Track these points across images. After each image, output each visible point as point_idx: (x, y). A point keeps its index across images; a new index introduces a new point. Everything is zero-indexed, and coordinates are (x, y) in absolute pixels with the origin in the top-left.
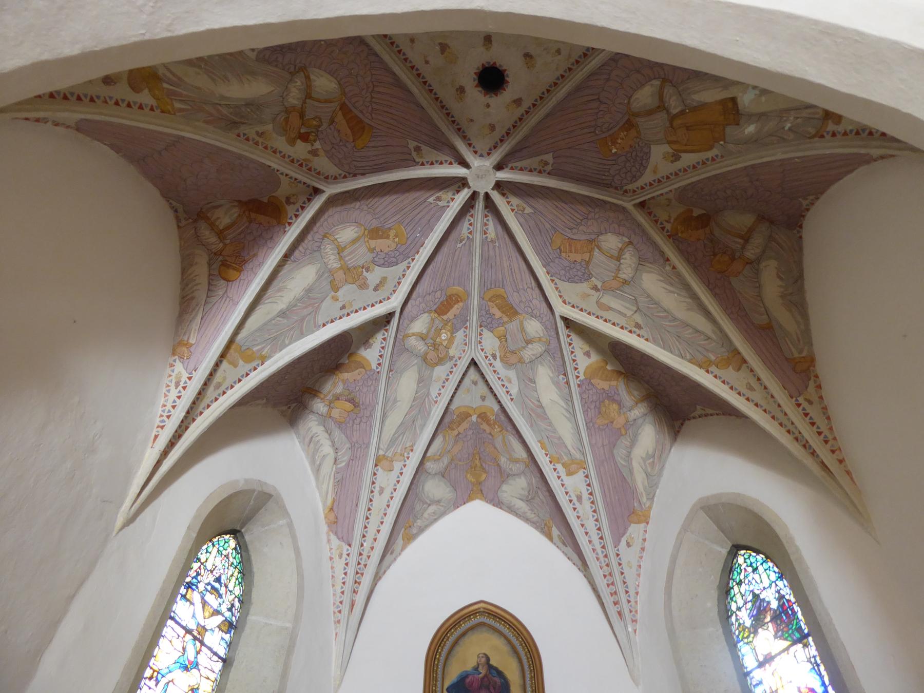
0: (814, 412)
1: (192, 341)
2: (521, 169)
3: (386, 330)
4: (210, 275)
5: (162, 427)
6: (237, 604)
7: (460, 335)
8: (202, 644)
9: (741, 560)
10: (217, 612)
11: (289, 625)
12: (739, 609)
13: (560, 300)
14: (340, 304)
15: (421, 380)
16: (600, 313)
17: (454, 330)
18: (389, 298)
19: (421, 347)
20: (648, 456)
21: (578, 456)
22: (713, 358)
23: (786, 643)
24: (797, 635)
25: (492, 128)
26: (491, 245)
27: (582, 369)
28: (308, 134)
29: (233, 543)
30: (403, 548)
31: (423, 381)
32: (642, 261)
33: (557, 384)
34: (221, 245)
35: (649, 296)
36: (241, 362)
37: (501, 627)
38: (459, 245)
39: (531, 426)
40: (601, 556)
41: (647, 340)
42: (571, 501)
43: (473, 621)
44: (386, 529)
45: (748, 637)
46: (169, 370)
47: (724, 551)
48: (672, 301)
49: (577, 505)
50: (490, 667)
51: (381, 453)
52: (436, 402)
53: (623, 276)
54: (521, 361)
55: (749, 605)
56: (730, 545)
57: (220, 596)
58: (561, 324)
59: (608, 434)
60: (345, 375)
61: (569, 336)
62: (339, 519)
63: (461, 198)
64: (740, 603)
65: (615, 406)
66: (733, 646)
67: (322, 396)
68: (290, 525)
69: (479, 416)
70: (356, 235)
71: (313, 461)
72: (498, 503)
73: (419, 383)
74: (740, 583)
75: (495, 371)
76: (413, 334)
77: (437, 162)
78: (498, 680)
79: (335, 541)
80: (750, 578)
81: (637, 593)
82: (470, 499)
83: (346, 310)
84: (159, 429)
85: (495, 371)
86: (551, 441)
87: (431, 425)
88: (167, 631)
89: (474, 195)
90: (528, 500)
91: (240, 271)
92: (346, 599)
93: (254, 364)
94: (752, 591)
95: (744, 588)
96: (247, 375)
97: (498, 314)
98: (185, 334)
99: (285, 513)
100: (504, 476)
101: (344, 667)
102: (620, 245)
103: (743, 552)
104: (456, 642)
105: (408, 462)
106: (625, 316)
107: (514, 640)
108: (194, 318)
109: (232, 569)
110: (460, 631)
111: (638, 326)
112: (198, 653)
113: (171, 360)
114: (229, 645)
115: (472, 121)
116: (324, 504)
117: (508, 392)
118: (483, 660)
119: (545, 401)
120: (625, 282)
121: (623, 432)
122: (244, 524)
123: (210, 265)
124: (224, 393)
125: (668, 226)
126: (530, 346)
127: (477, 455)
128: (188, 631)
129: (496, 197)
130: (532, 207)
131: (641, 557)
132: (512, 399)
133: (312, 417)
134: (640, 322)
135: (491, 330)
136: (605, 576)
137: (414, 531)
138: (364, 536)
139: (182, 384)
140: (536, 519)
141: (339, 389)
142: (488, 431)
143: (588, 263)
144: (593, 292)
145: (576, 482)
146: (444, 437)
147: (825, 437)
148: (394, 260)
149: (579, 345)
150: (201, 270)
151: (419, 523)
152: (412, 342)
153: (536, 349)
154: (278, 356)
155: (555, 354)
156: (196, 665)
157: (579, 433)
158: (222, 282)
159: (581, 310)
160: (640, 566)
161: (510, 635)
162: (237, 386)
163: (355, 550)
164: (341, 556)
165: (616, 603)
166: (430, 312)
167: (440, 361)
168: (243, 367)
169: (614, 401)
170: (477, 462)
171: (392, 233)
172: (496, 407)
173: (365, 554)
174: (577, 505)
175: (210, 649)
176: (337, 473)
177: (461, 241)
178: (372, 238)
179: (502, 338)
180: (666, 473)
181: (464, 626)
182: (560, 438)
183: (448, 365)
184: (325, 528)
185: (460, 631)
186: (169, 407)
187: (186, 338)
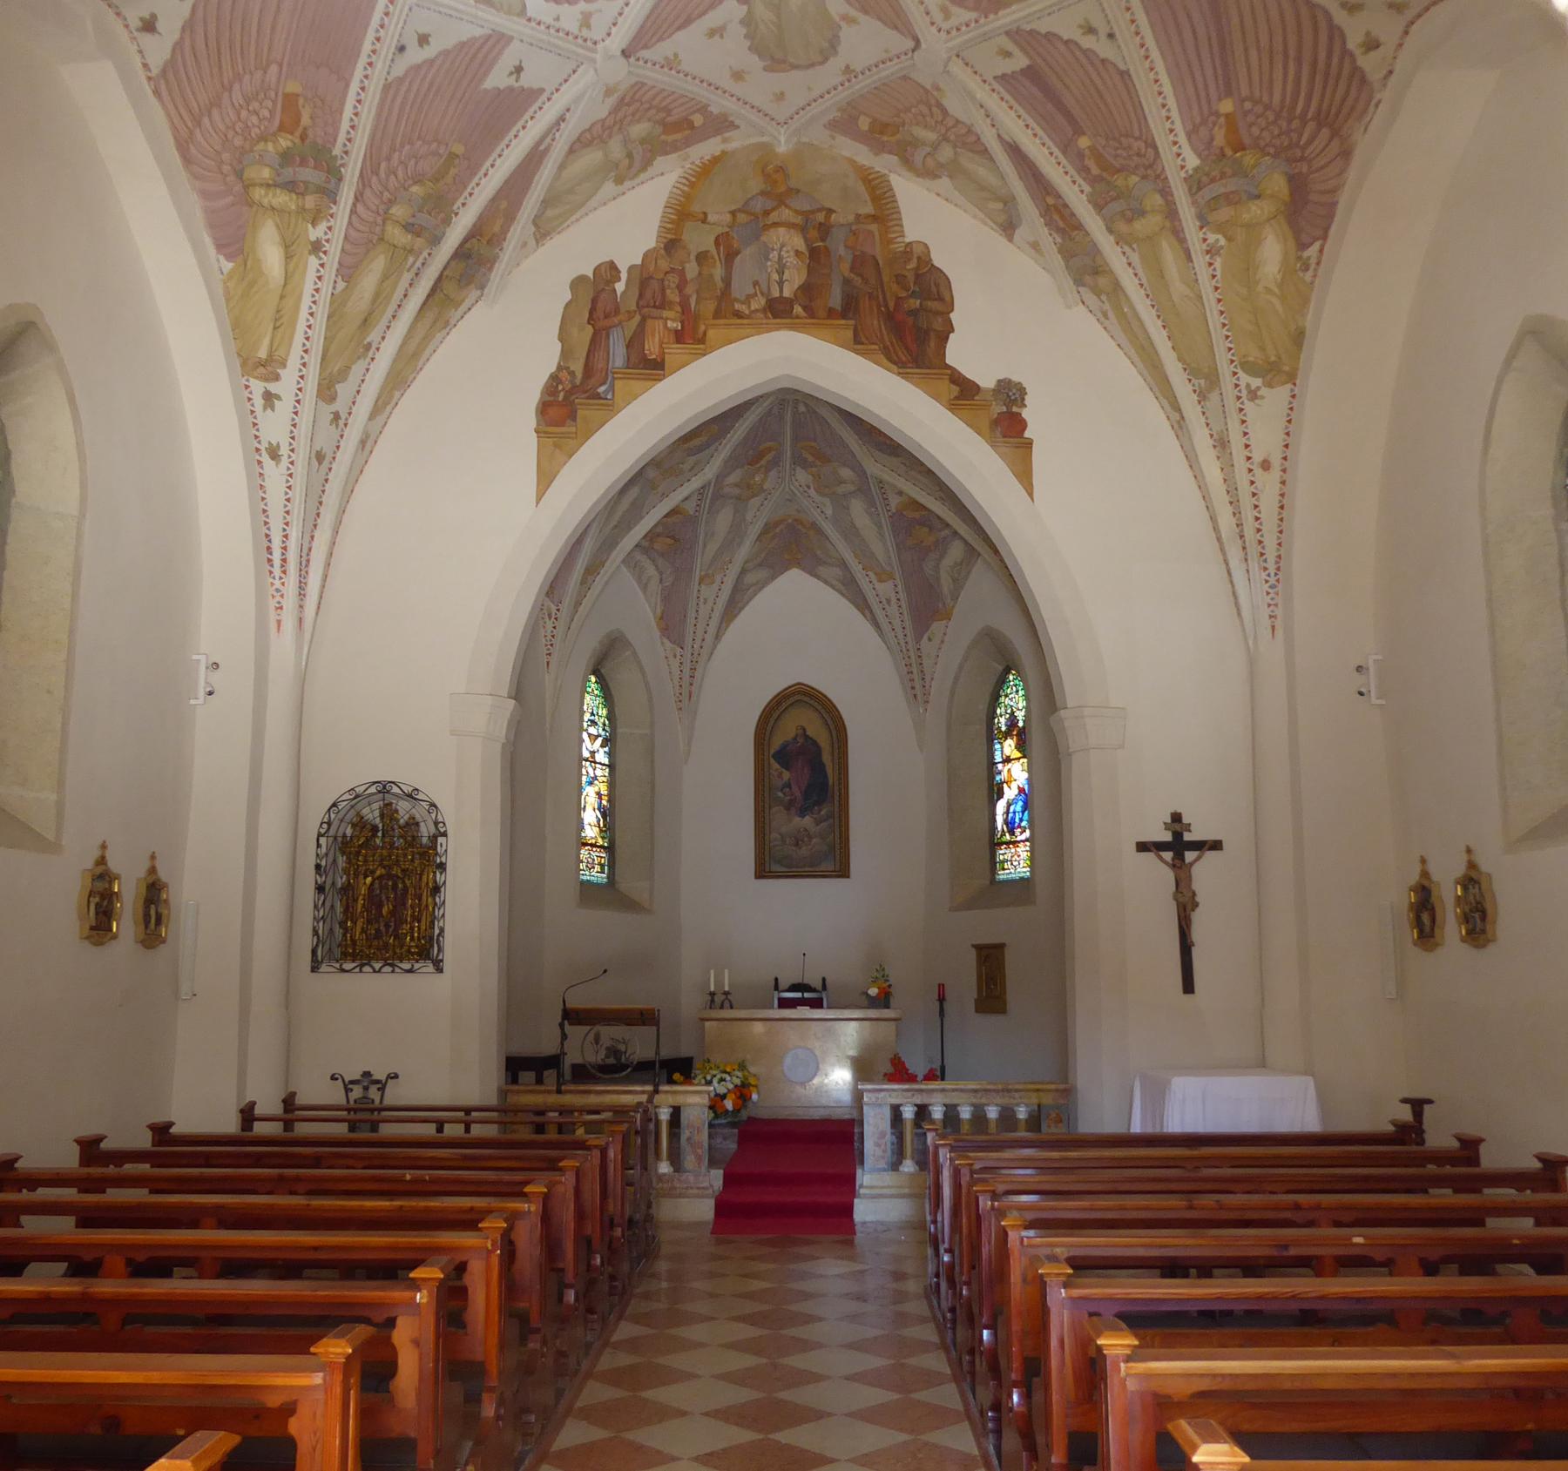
7: (773, 473)
17: (768, 471)
19: (737, 491)
23: (1019, 755)
43: (792, 700)
44: (714, 623)
47: (1001, 668)
62: (671, 625)
65: (926, 529)
68: (635, 654)
71: (639, 580)
95: (1007, 701)
97: (810, 459)
119: (858, 523)
145: (885, 588)
156: (595, 778)
181: (784, 705)
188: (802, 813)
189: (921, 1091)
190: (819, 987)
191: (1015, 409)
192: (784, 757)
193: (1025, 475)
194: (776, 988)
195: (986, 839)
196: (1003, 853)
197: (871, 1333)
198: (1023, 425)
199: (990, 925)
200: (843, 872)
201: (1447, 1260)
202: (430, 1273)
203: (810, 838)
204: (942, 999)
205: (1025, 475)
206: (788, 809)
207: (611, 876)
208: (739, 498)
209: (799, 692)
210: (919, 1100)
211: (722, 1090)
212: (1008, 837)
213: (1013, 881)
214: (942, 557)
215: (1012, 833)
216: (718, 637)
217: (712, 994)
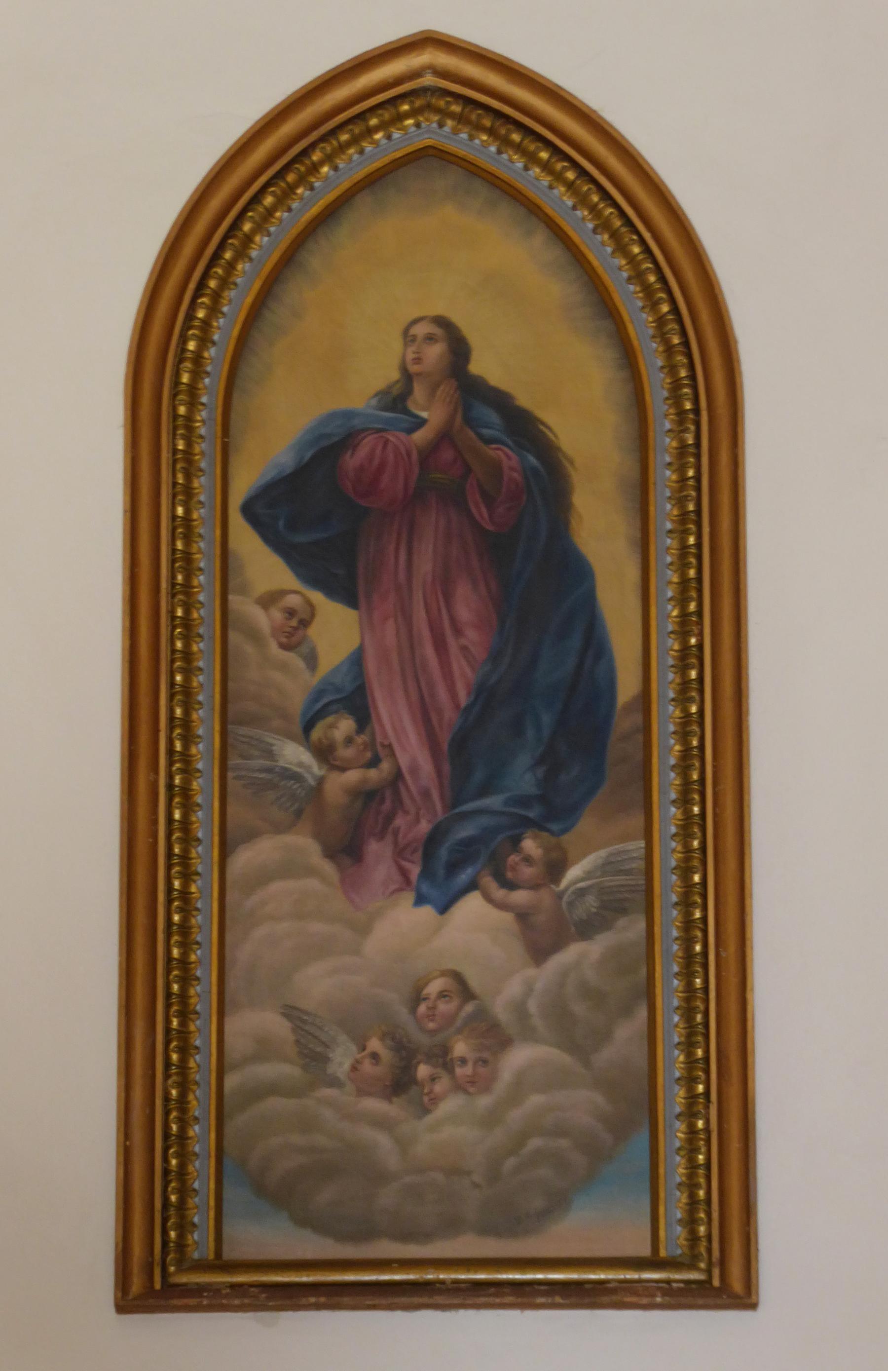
37: (535, 181)
43: (382, 147)
50: (471, 391)
78: (509, 459)
104: (290, 259)
107: (600, 251)
110: (307, 204)
118: (435, 352)
161: (580, 224)
181: (330, 180)
185: (307, 204)
188: (442, 872)
192: (325, 512)
197: (243, 730)
201: (614, 1291)
202: (131, 1297)
203: (494, 1038)
206: (346, 851)
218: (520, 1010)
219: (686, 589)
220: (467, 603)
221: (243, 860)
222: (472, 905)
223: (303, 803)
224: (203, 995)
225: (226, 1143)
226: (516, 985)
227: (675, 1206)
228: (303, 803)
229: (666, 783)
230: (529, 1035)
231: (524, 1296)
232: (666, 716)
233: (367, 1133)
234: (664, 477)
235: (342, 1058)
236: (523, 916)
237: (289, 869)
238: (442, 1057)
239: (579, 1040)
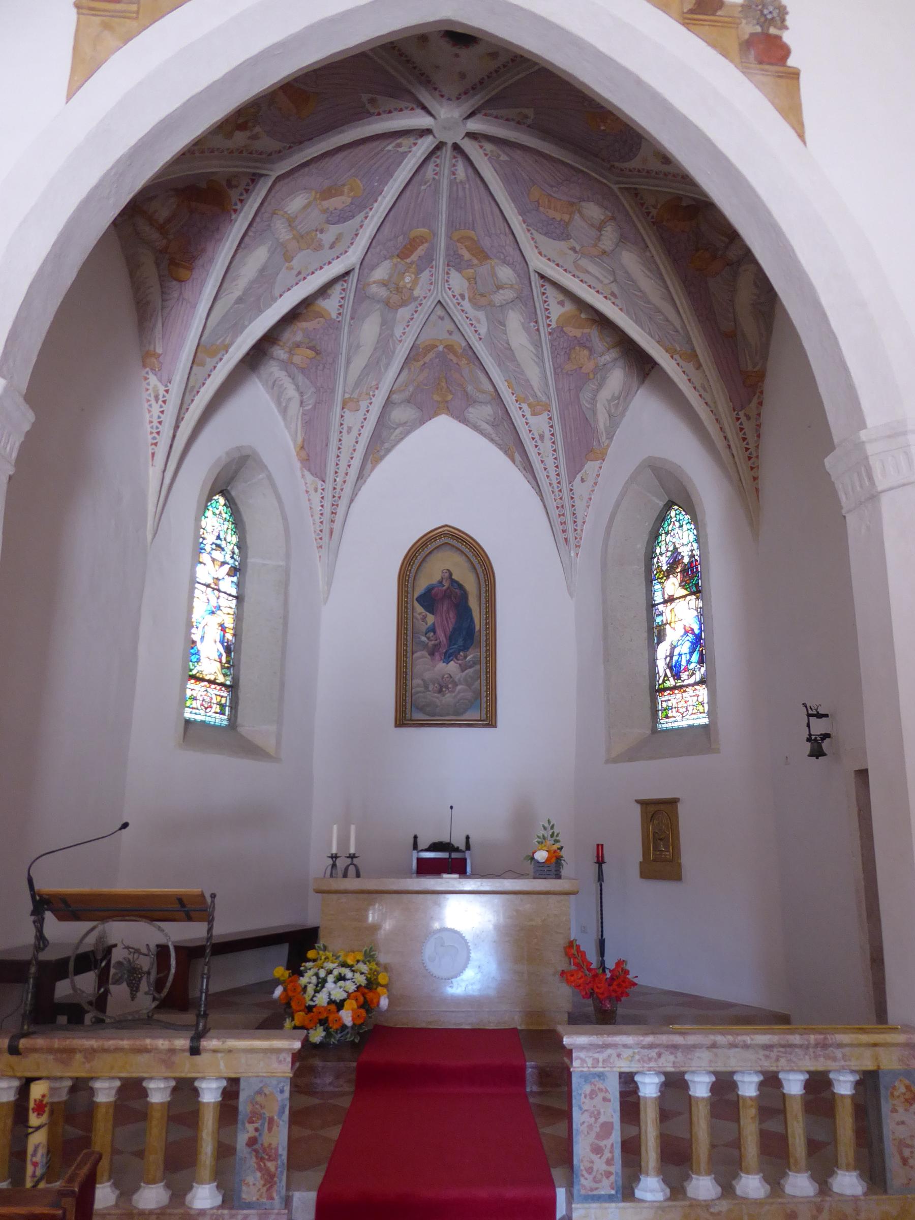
0: (748, 426)
1: (159, 350)
2: (496, 117)
3: (345, 281)
4: (160, 277)
5: (156, 444)
6: (236, 551)
7: (425, 275)
8: (219, 590)
9: (673, 513)
10: (223, 563)
11: (282, 563)
12: (661, 554)
13: (536, 251)
14: (295, 272)
15: (384, 323)
16: (577, 273)
17: (419, 271)
18: (346, 252)
19: (383, 293)
20: (614, 398)
21: (544, 399)
22: (678, 349)
23: (685, 592)
24: (694, 589)
25: (463, 76)
26: (460, 186)
27: (554, 316)
28: (246, 123)
29: (222, 501)
30: (372, 469)
31: (386, 324)
32: (623, 239)
33: (526, 329)
34: (165, 241)
35: (626, 272)
36: (208, 360)
37: (463, 548)
38: (423, 187)
39: (499, 366)
40: (556, 490)
41: (621, 309)
42: (533, 439)
44: (356, 463)
45: (662, 578)
46: (144, 383)
47: (661, 504)
48: (647, 284)
49: (539, 443)
50: (453, 581)
51: (347, 396)
52: (400, 341)
53: (603, 247)
54: (491, 304)
55: (669, 554)
56: (667, 499)
57: (223, 549)
58: (534, 278)
59: (574, 380)
60: (304, 325)
61: (543, 286)
62: (312, 456)
63: (425, 146)
64: (664, 549)
65: (586, 352)
66: (649, 582)
67: (281, 344)
68: (270, 477)
69: (445, 347)
70: (306, 201)
71: (278, 403)
72: (464, 421)
73: (382, 325)
74: (667, 533)
75: (463, 311)
76: (374, 282)
77: (395, 109)
79: (309, 477)
80: (675, 532)
81: (584, 523)
82: (436, 414)
83: (301, 276)
84: (153, 446)
85: (463, 311)
86: (518, 380)
87: (396, 365)
88: (197, 593)
89: (440, 146)
90: (494, 426)
91: (191, 269)
92: (326, 527)
93: (219, 356)
94: (674, 543)
95: (669, 538)
96: (215, 367)
97: (467, 255)
98: (150, 343)
99: (264, 467)
100: (470, 401)
101: (329, 584)
102: (603, 218)
103: (676, 507)
104: (424, 560)
105: (373, 400)
106: (601, 282)
107: (473, 559)
108: (154, 325)
109: (226, 523)
110: (427, 551)
111: (613, 294)
112: (218, 598)
113: (143, 373)
114: (238, 585)
115: (437, 67)
116: (295, 441)
117: (476, 331)
118: (447, 575)
119: (514, 344)
120: (604, 252)
121: (591, 376)
122: (229, 483)
123: (157, 265)
124: (198, 392)
125: (654, 212)
126: (501, 291)
127: (443, 380)
128: (208, 586)
129: (469, 146)
130: (508, 155)
131: (593, 491)
132: (480, 339)
133: (272, 363)
134: (616, 292)
135: (459, 270)
136: (558, 507)
137: (382, 453)
138: (336, 472)
139: (161, 399)
140: (500, 442)
141: (299, 337)
142: (455, 361)
143: (567, 224)
144: (571, 252)
145: (540, 423)
146: (410, 369)
147: (751, 453)
148: (351, 214)
149: (553, 295)
150: (149, 271)
151: (386, 445)
152: (374, 289)
153: (508, 294)
154: (239, 340)
155: (525, 300)
156: (219, 608)
157: (546, 378)
158: (175, 283)
159: (558, 265)
160: (590, 499)
161: (470, 555)
162: (208, 382)
163: (329, 485)
164: (316, 490)
165: (564, 531)
166: (391, 258)
167: (404, 303)
168: (210, 362)
169: (586, 347)
170: (443, 384)
171: (346, 189)
172: (464, 344)
173: (338, 488)
174: (539, 443)
175: (225, 593)
176: (303, 414)
177: (426, 183)
178: (325, 199)
179: (472, 280)
180: (628, 414)
181: (431, 547)
182: (527, 381)
183: (413, 306)
184: (298, 465)
185: (427, 551)
186: (155, 424)
187: (152, 348)
188: (448, 657)
189: (674, 1047)
190: (463, 847)
191: (773, 31)
192: (429, 600)
193: (792, 111)
194: (415, 846)
195: (646, 684)
196: (667, 700)
198: (785, 52)
199: (656, 778)
200: (490, 721)
204: (600, 861)
205: (792, 111)
206: (432, 654)
207: (233, 719)
208: (387, 303)
209: (445, 535)
210: (668, 1063)
211: (338, 995)
212: (671, 682)
213: (672, 730)
214: (600, 386)
215: (677, 676)
216: (361, 476)
217: (334, 857)
218: (459, 680)
219: (487, 602)
220: (452, 615)
221: (415, 655)
222: (452, 663)
223: (425, 646)
224: (409, 677)
225: (409, 895)
226: (458, 676)
227: (484, 712)
228: (425, 646)
229: (483, 644)
230: (461, 684)
231: (460, 725)
232: (483, 633)
233: (434, 699)
234: (483, 595)
235: (431, 687)
236: (460, 665)
237: (423, 657)
238: (447, 688)
239: (469, 685)
